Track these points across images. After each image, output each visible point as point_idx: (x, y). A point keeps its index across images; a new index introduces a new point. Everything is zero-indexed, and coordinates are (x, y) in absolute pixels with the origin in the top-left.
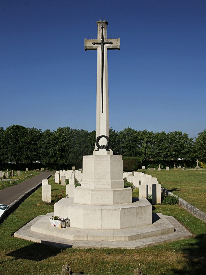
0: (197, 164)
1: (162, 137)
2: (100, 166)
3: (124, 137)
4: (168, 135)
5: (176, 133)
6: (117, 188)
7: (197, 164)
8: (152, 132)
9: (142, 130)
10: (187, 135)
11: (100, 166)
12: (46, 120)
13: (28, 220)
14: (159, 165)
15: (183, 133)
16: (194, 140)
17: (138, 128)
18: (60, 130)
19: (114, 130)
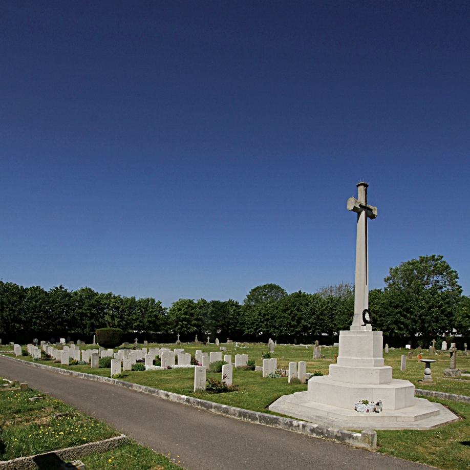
0: (178, 339)
1: (132, 304)
2: (360, 342)
3: (81, 301)
4: (139, 302)
5: (148, 300)
6: (427, 359)
7: (178, 339)
8: (119, 296)
9: (107, 293)
10: (161, 303)
11: (360, 342)
12: (304, 279)
13: (275, 395)
14: (434, 340)
15: (156, 301)
16: (168, 311)
17: (100, 289)
18: (298, 295)
19: (66, 289)
